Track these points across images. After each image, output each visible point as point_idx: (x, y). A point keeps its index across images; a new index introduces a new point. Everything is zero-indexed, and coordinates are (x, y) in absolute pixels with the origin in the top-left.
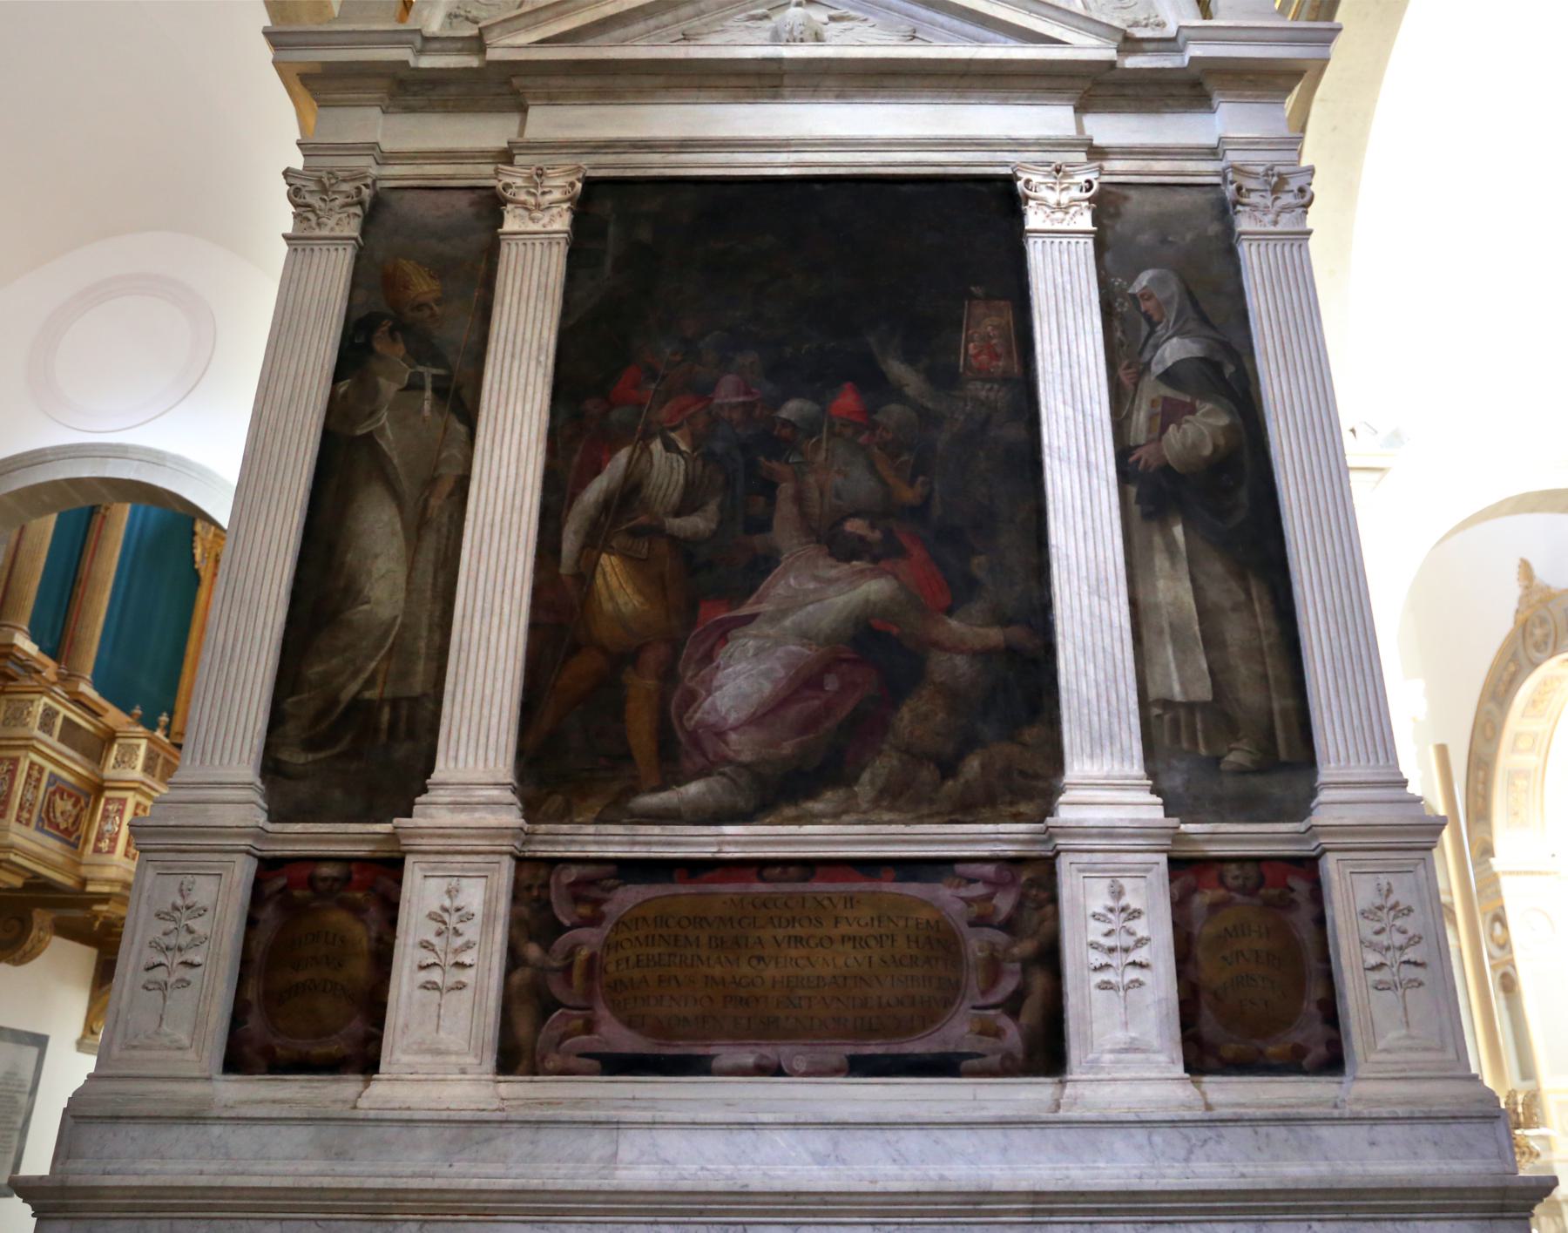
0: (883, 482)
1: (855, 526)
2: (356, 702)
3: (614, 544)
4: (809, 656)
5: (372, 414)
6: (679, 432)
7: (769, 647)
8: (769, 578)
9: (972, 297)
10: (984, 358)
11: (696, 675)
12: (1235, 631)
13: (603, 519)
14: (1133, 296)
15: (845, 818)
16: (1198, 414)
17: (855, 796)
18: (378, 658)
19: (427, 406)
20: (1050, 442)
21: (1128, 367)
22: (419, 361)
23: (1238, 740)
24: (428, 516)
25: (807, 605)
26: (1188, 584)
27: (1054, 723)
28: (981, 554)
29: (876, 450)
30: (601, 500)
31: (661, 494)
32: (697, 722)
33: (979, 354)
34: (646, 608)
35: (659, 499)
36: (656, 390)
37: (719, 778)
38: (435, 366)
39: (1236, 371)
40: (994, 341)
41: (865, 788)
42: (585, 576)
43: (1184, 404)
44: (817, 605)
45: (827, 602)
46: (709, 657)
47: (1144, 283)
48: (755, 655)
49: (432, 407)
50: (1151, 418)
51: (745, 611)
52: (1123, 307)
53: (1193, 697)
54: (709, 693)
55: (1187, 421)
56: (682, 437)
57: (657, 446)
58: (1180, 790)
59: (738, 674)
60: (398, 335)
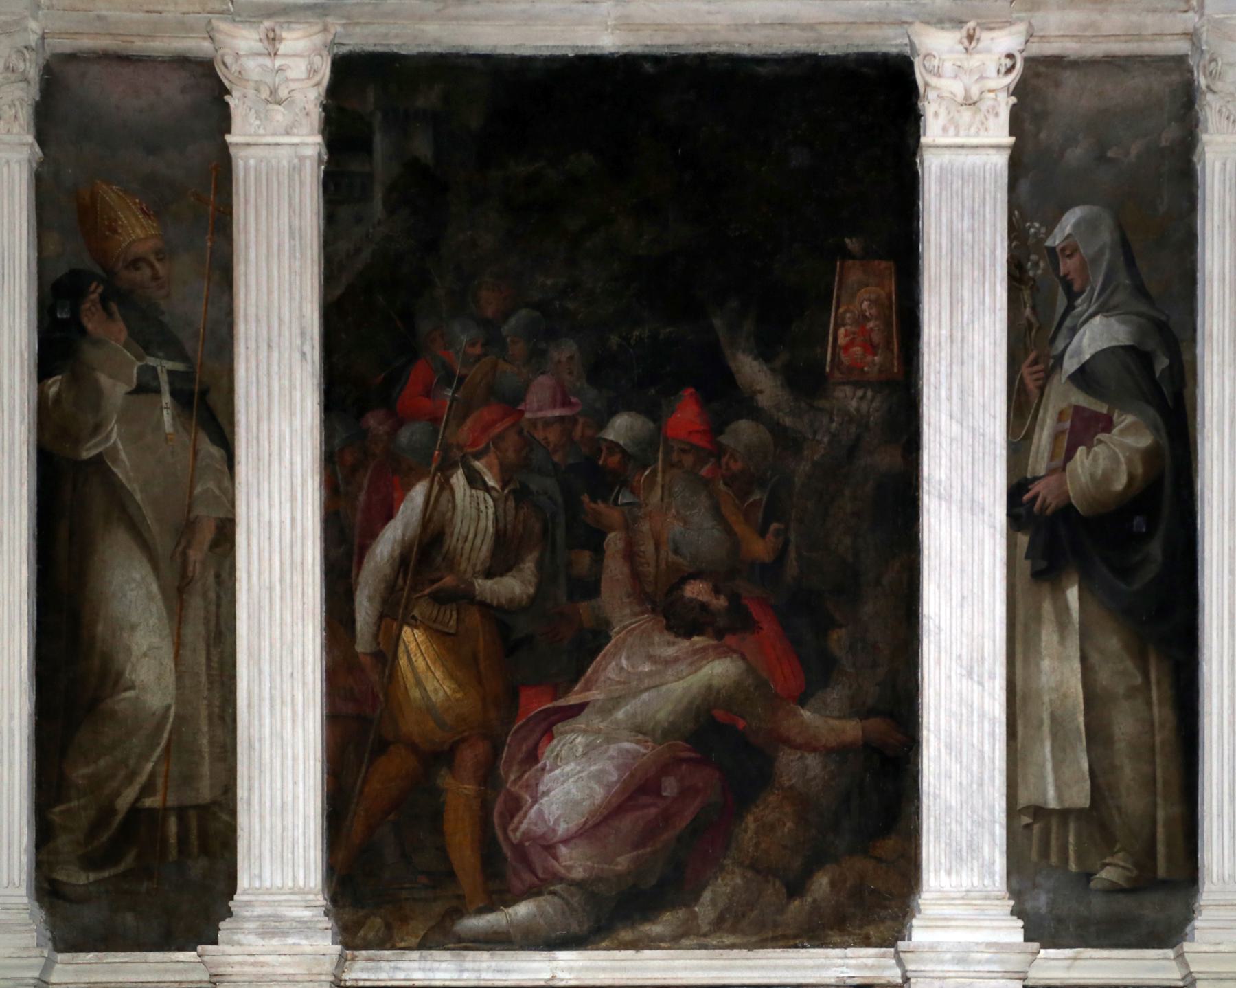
0: (729, 530)
1: (695, 590)
2: (135, 811)
3: (416, 613)
4: (644, 755)
5: (97, 428)
6: (484, 461)
7: (600, 745)
8: (598, 658)
9: (847, 255)
10: (857, 350)
11: (520, 777)
12: (1124, 725)
13: (400, 582)
14: (1052, 250)
15: (684, 941)
16: (1115, 431)
17: (695, 916)
18: (154, 758)
19: (167, 417)
20: (929, 475)
21: (1035, 362)
22: (147, 349)
23: (1113, 854)
24: (190, 575)
25: (642, 691)
26: (1077, 665)
27: (912, 837)
28: (840, 626)
29: (722, 486)
30: (397, 553)
31: (468, 545)
32: (524, 833)
33: (852, 343)
34: (459, 695)
35: (466, 555)
36: (453, 399)
37: (549, 897)
38: (169, 358)
39: (1170, 366)
40: (871, 324)
41: (705, 910)
42: (386, 656)
43: (1096, 416)
44: (653, 693)
45: (664, 688)
46: (533, 757)
47: (1068, 230)
48: (584, 754)
49: (173, 418)
50: (1056, 437)
51: (573, 699)
52: (1037, 269)
53: (1067, 805)
54: (535, 801)
55: (1100, 442)
56: (490, 467)
57: (459, 479)
58: (1044, 910)
59: (568, 776)
60: (114, 307)
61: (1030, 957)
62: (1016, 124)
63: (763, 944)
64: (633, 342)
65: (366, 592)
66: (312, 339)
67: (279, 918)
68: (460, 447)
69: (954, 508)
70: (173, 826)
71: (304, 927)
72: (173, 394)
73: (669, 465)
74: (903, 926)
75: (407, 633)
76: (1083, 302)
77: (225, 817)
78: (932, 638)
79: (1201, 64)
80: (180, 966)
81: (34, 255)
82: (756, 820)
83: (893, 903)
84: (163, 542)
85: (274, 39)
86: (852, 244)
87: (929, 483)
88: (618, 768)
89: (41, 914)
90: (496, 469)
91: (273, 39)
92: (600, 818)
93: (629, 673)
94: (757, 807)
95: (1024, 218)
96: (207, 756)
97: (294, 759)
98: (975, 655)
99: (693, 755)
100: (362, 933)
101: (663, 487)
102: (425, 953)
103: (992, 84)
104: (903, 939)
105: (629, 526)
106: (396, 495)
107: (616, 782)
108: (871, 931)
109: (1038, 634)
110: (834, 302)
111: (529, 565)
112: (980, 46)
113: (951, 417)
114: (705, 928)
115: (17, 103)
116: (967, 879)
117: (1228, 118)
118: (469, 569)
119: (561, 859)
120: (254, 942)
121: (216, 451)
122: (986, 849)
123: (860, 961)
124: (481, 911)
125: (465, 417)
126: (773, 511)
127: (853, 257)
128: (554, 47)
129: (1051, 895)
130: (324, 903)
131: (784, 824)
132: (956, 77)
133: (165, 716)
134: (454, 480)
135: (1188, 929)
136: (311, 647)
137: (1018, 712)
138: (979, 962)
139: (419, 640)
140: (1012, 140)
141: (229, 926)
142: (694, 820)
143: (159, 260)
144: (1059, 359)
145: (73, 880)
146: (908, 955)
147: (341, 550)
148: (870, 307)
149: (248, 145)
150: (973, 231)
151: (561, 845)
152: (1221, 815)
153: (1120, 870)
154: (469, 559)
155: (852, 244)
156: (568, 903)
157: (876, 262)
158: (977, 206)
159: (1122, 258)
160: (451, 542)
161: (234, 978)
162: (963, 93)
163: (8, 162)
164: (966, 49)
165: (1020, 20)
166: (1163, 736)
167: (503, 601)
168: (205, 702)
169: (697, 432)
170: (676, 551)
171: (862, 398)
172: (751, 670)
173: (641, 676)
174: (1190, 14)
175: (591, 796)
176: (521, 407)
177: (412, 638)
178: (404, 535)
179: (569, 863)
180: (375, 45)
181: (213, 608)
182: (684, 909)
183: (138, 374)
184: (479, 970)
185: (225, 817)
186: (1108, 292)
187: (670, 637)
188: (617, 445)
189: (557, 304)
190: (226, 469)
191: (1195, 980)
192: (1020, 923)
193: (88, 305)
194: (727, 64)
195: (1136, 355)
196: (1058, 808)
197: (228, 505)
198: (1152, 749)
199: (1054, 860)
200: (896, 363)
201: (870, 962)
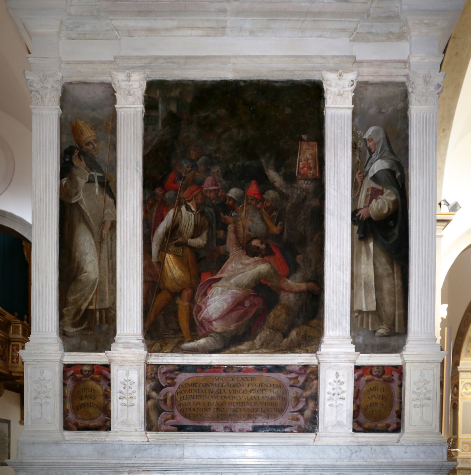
0: (266, 224)
1: (255, 243)
2: (87, 310)
3: (170, 249)
4: (239, 294)
5: (77, 193)
6: (191, 202)
9: (302, 140)
11: (201, 300)
12: (386, 285)
14: (365, 140)
15: (251, 351)
16: (384, 195)
17: (254, 344)
19: (97, 190)
21: (360, 173)
22: (91, 169)
23: (382, 325)
24: (103, 238)
26: (372, 267)
27: (321, 319)
28: (300, 254)
29: (264, 211)
30: (164, 231)
31: (186, 229)
32: (202, 318)
33: (304, 167)
34: (183, 275)
36: (182, 184)
40: (310, 161)
41: (258, 341)
42: (161, 263)
45: (245, 273)
46: (205, 294)
47: (370, 133)
48: (221, 293)
49: (99, 190)
50: (366, 196)
51: (218, 276)
52: (361, 145)
53: (369, 309)
54: (206, 308)
55: (380, 198)
56: (193, 205)
57: (183, 208)
58: (361, 342)
60: (82, 157)
61: (357, 356)
62: (354, 102)
63: (275, 352)
64: (237, 166)
65: (155, 243)
66: (140, 166)
67: (129, 343)
68: (184, 198)
69: (335, 218)
70: (98, 315)
71: (136, 346)
72: (99, 183)
73: (248, 204)
74: (318, 347)
75: (167, 256)
76: (374, 156)
77: (113, 312)
78: (328, 258)
79: (410, 84)
80: (100, 357)
81: (59, 142)
82: (273, 314)
83: (315, 340)
84: (96, 228)
85: (129, 76)
86: (304, 137)
87: (327, 210)
88: (231, 298)
89: (60, 341)
90: (195, 205)
91: (129, 76)
92: (226, 313)
93: (235, 268)
94: (274, 310)
95: (356, 130)
96: (108, 293)
97: (133, 294)
98: (341, 263)
99: (254, 294)
100: (153, 348)
101: (246, 210)
102: (172, 354)
103: (347, 89)
104: (318, 351)
105: (235, 223)
106: (164, 213)
107: (231, 302)
108: (309, 348)
109: (360, 257)
110: (299, 154)
111: (205, 235)
112: (343, 78)
113: (334, 190)
114: (258, 347)
115: (55, 97)
116: (338, 333)
117: (418, 101)
118: (186, 236)
119: (214, 326)
120: (121, 350)
121: (111, 200)
122: (344, 323)
123: (305, 358)
124: (189, 341)
125: (185, 190)
126: (280, 218)
127: (304, 141)
128: (213, 77)
129: (364, 338)
130: (142, 338)
131: (282, 315)
132: (336, 87)
133: (96, 281)
134: (182, 209)
135: (404, 348)
136: (139, 259)
137: (354, 281)
138: (341, 358)
139: (171, 258)
140: (353, 106)
141: (114, 345)
142: (254, 314)
143: (96, 143)
144: (367, 172)
145: (69, 331)
146: (320, 356)
147: (148, 230)
148: (310, 156)
149: (121, 108)
150: (341, 133)
151: (214, 321)
152: (415, 313)
153: (384, 330)
154: (186, 233)
155: (304, 137)
156: (215, 339)
157: (312, 142)
158: (342, 126)
159: (386, 142)
160: (181, 228)
161: (116, 361)
162: (338, 92)
163: (52, 114)
164: (339, 79)
165: (355, 70)
166: (398, 288)
167: (197, 246)
168: (107, 277)
169: (256, 194)
170: (250, 230)
171: (307, 184)
172: (272, 267)
173: (239, 269)
174: (406, 70)
175: (223, 306)
176: (202, 186)
177: (169, 258)
178: (167, 226)
179: (216, 327)
180: (159, 77)
181: (110, 248)
182: (251, 341)
183: (89, 177)
184: (189, 360)
185: (113, 312)
186: (382, 152)
187: (248, 257)
188: (232, 198)
189: (214, 155)
190: (114, 206)
191: (406, 363)
192: (354, 346)
193: (74, 157)
194: (266, 83)
195: (391, 172)
196: (366, 310)
197: (115, 217)
198: (395, 293)
199: (364, 326)
200: (317, 173)
201: (308, 358)
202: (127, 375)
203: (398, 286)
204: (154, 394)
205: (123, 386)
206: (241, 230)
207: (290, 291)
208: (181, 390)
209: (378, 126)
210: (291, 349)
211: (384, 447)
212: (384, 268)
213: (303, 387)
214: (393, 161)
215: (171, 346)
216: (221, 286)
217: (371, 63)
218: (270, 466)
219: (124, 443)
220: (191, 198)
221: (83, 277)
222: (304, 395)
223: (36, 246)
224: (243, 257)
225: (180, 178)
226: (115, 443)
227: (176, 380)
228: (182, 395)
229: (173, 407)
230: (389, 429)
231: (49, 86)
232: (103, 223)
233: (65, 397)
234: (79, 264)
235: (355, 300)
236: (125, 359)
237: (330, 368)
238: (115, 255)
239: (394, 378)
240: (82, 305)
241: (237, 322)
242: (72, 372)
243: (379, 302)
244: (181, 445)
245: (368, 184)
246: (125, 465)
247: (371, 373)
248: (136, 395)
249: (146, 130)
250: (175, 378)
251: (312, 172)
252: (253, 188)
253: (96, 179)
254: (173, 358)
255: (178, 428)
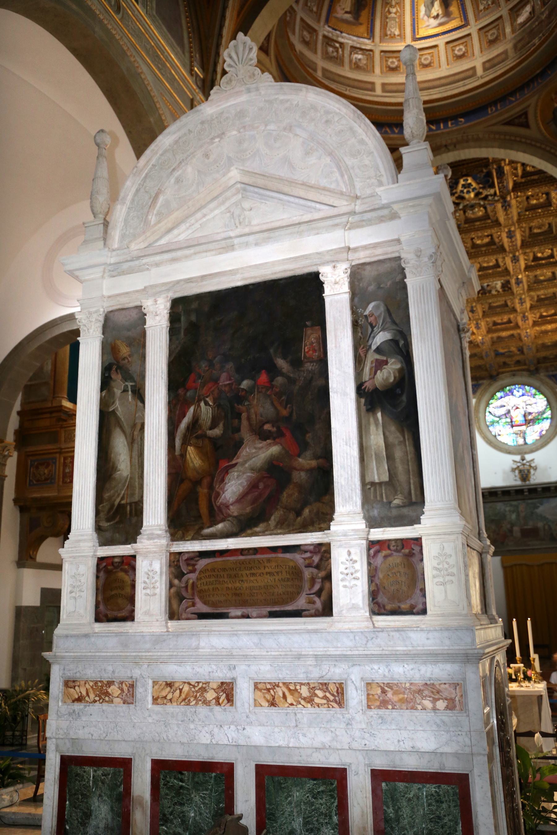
0: (275, 408)
1: (267, 427)
2: (119, 505)
3: (191, 442)
5: (113, 403)
12: (398, 454)
15: (266, 533)
16: (389, 364)
17: (269, 525)
19: (130, 397)
21: (363, 348)
28: (309, 432)
29: (273, 396)
33: (309, 351)
36: (201, 382)
40: (314, 344)
41: (272, 522)
42: (183, 455)
46: (223, 480)
47: (370, 309)
48: (237, 478)
50: (371, 369)
51: (234, 462)
52: (361, 321)
54: (223, 493)
56: (210, 399)
57: (202, 404)
60: (119, 371)
63: (289, 533)
67: (152, 534)
71: (159, 537)
73: (259, 392)
75: (189, 448)
77: (141, 505)
86: (308, 323)
88: (246, 481)
89: (95, 535)
90: (212, 400)
91: (156, 301)
95: (357, 308)
105: (248, 411)
109: (369, 428)
111: (221, 425)
116: (349, 508)
121: (141, 405)
124: (209, 527)
133: (127, 477)
134: (201, 404)
138: (351, 535)
144: (370, 346)
155: (308, 323)
156: (232, 523)
160: (201, 421)
171: (313, 366)
172: (284, 448)
175: (239, 490)
177: (191, 449)
187: (260, 441)
195: (394, 342)
198: (408, 461)
199: (378, 498)
201: (320, 536)
202: (151, 565)
203: (410, 453)
204: (176, 582)
205: (147, 576)
206: (254, 416)
207: (301, 470)
208: (201, 576)
209: (377, 300)
210: (304, 528)
211: (402, 633)
212: (395, 436)
213: (318, 567)
214: (395, 331)
215: (191, 533)
216: (237, 471)
217: (365, 248)
218: (280, 657)
219: (145, 634)
220: (208, 394)
221: (117, 475)
222: (320, 575)
223: (78, 453)
224: (257, 442)
225: (199, 378)
226: (137, 634)
227: (196, 567)
228: (202, 581)
229: (193, 594)
230: (414, 611)
231: (94, 320)
232: (134, 425)
233: (97, 589)
234: (114, 463)
235: (366, 472)
236: (149, 550)
237: (340, 546)
238: (144, 452)
239: (414, 552)
240: (115, 500)
241: (252, 505)
242: (104, 564)
243: (392, 472)
244: (194, 634)
245: (372, 357)
246: (144, 657)
247: (389, 548)
248: (158, 584)
249: (170, 340)
250: (195, 565)
251: (317, 354)
252: (263, 377)
253: (129, 387)
254: (193, 545)
255: (198, 616)
